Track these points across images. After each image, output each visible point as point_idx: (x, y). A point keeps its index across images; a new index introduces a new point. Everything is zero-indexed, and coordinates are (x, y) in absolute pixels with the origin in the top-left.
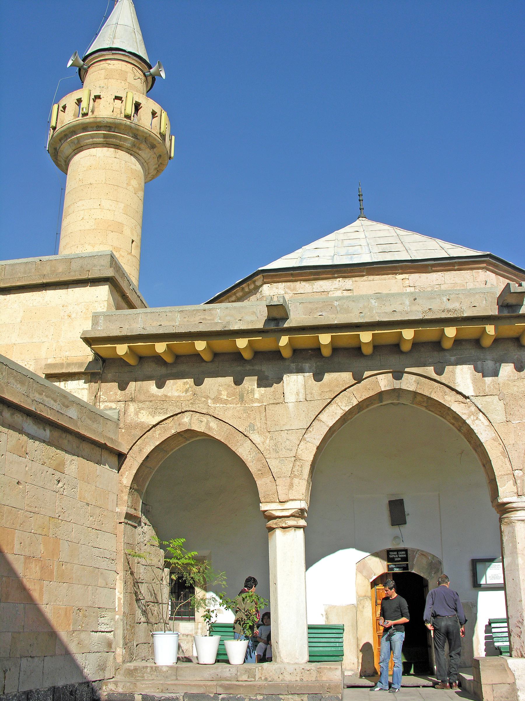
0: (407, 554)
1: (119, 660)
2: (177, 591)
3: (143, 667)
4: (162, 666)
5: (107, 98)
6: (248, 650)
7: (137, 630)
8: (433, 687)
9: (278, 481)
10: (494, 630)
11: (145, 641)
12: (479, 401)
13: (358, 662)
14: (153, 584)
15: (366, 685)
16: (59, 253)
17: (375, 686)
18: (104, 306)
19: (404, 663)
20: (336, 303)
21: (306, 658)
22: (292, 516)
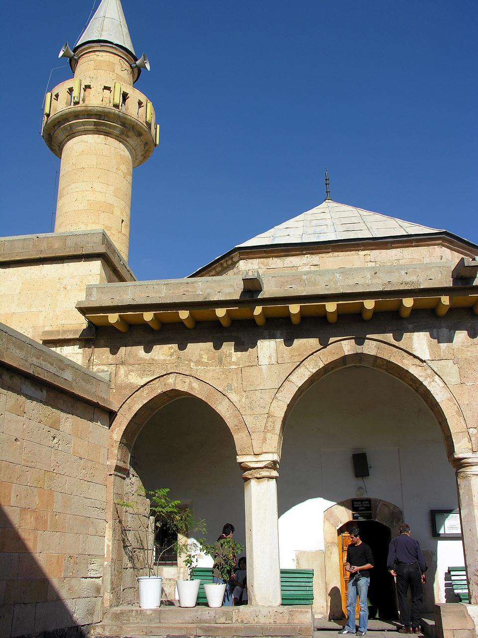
0: (370, 503)
1: (107, 604)
2: (161, 538)
3: (129, 611)
4: (147, 610)
5: (97, 87)
6: (226, 593)
7: (124, 575)
8: (397, 631)
9: (252, 435)
10: (453, 578)
11: (131, 586)
12: (434, 365)
13: (327, 606)
14: (140, 532)
15: (335, 628)
16: (55, 230)
17: (343, 629)
18: (97, 279)
19: (369, 608)
20: (304, 277)
21: (279, 601)
22: (265, 467)
